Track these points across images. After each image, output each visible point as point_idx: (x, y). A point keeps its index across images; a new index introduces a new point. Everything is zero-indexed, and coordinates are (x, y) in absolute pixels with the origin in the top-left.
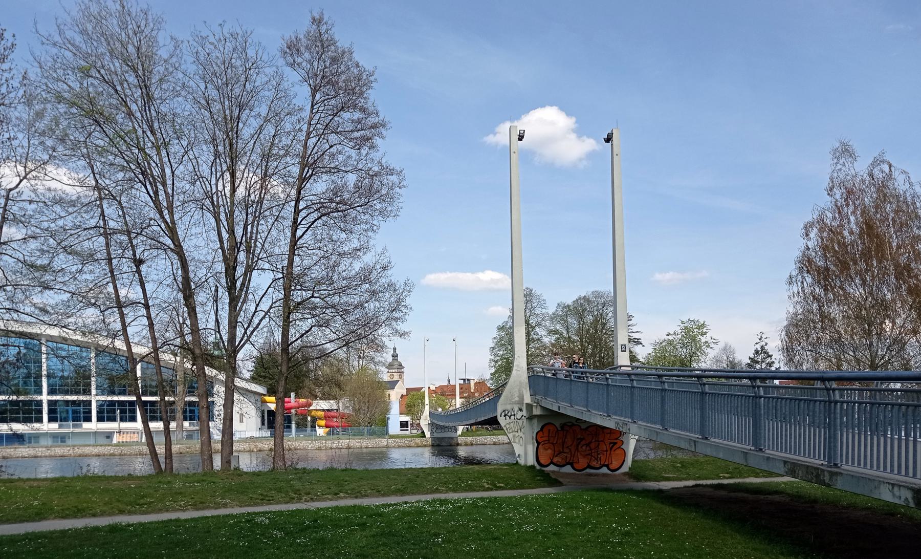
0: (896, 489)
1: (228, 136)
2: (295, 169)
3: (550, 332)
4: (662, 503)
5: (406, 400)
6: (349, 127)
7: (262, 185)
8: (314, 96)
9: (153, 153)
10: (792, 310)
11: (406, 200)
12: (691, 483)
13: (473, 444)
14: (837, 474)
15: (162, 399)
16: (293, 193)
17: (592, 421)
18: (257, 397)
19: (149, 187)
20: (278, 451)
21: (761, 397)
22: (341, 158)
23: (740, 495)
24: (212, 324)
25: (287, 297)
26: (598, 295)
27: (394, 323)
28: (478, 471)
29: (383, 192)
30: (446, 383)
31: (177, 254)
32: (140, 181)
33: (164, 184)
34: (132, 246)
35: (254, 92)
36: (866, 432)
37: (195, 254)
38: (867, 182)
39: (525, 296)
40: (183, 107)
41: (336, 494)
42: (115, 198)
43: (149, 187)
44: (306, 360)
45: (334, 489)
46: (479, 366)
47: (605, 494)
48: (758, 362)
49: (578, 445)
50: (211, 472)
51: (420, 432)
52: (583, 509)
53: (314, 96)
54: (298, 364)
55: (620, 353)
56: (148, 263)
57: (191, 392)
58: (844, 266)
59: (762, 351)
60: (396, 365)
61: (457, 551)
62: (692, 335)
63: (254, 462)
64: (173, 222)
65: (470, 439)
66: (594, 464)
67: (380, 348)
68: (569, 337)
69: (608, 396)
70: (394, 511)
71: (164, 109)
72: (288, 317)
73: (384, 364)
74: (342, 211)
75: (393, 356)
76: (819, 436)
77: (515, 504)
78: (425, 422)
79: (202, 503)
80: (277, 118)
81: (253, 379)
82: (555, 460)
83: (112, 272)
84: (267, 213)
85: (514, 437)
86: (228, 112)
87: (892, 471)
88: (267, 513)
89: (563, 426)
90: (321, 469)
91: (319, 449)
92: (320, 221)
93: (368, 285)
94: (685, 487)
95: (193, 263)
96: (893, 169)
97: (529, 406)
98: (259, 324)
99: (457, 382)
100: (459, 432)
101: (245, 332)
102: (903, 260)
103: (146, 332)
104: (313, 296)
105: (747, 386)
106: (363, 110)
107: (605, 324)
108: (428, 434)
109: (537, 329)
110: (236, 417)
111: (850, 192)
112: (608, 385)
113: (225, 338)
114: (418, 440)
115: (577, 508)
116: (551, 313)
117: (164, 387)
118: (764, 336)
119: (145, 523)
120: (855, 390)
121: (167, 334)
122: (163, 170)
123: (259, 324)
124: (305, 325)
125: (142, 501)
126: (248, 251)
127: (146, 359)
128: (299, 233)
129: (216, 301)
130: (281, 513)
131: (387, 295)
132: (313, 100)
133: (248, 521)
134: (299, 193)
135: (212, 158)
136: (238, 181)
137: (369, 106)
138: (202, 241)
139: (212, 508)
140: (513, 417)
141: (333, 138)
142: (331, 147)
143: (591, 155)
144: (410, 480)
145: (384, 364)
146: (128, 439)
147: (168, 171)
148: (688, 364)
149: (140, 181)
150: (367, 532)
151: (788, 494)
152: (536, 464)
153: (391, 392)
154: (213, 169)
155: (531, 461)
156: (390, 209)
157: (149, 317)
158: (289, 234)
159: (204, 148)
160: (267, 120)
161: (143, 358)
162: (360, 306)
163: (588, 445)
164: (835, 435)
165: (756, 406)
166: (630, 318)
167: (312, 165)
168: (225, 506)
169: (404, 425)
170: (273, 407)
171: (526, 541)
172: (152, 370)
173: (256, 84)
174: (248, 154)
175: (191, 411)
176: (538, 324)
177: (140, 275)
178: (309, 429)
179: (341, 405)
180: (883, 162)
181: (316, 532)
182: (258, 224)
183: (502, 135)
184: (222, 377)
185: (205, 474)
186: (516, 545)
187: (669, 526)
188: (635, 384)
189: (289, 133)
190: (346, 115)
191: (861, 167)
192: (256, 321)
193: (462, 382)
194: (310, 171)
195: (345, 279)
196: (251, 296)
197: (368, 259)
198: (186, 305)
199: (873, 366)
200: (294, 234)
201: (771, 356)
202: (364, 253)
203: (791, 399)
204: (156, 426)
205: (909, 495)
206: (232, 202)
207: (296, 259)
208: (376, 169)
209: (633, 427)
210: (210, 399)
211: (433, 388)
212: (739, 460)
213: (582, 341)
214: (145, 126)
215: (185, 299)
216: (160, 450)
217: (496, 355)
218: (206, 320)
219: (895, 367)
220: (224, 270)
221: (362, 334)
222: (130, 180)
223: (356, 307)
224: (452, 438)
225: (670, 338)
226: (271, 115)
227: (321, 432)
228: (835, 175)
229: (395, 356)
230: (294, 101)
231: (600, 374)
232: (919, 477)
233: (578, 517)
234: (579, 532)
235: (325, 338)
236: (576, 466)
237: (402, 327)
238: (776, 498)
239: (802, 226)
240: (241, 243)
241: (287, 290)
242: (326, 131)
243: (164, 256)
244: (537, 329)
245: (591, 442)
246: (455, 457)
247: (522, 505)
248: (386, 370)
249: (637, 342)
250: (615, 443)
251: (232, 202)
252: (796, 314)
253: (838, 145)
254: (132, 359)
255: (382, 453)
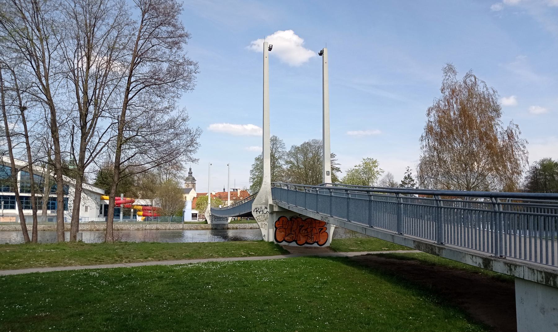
0: (474, 258)
1: (87, 35)
2: (129, 57)
3: (287, 162)
4: (347, 265)
5: (197, 201)
6: (165, 35)
7: (107, 65)
8: (143, 15)
9: (37, 43)
10: (423, 156)
11: (199, 80)
12: (365, 253)
13: (245, 231)
14: (442, 248)
15: (33, 195)
16: (128, 72)
17: (308, 215)
18: (96, 196)
19: (33, 63)
20: (108, 231)
21: (401, 204)
22: (159, 53)
23: (392, 260)
24: (68, 149)
25: (120, 134)
26: (316, 142)
27: (189, 153)
28: (239, 245)
29: (185, 75)
30: (222, 191)
31: (49, 105)
32: (28, 59)
33: (44, 62)
34: (20, 98)
35: (106, 11)
36: (461, 225)
37: (60, 105)
38: (463, 86)
39: (272, 140)
40: (59, 16)
41: (146, 258)
42: (10, 69)
43: (33, 63)
44: (132, 173)
45: (145, 255)
46: (242, 181)
47: (314, 259)
48: (406, 184)
49: (300, 230)
50: (64, 243)
51: (204, 220)
52: (300, 268)
53: (143, 15)
54: (126, 176)
55: (326, 176)
56: (29, 109)
57: (53, 192)
58: (450, 132)
59: (409, 177)
60: (191, 179)
61: (220, 294)
62: (369, 168)
63: (92, 238)
64: (48, 85)
65: (236, 225)
66: (309, 241)
67: (179, 168)
68: (298, 166)
69: (331, 202)
70: (182, 269)
71: (46, 17)
72: (120, 147)
73: (183, 178)
74: (158, 85)
75: (189, 173)
76: (433, 226)
77: (259, 265)
78: (207, 215)
79: (55, 262)
80: (120, 27)
81: (96, 185)
82: (286, 238)
83: (4, 114)
84: (110, 83)
85: (262, 224)
86: (88, 21)
87: (472, 248)
88: (98, 269)
89: (291, 219)
90: (137, 242)
91: (138, 230)
92: (144, 90)
93: (173, 130)
94: (362, 255)
95: (58, 111)
96: (477, 80)
97: (271, 206)
98: (100, 151)
99: (229, 190)
100: (229, 221)
101: (91, 155)
102: (483, 130)
103: (25, 152)
104: (137, 135)
105: (397, 198)
106: (174, 26)
107: (319, 159)
108: (209, 222)
109: (279, 160)
110: (82, 209)
111: (453, 91)
112: (317, 194)
113: (77, 158)
114: (203, 226)
115: (296, 267)
116: (288, 151)
117: (33, 186)
118: (410, 169)
119: (14, 275)
120: (459, 201)
121: (39, 155)
122: (44, 53)
123: (100, 151)
124: (130, 153)
125: (14, 261)
126: (96, 105)
127: (24, 169)
128: (130, 96)
129: (73, 135)
130: (107, 270)
131: (185, 136)
132: (143, 18)
133: (85, 275)
134: (131, 72)
135: (76, 48)
136: (91, 63)
137: (178, 24)
138: (65, 98)
139: (62, 266)
140: (261, 212)
141: (154, 41)
142: (153, 46)
143: (311, 59)
144: (195, 250)
145: (183, 178)
146: (9, 221)
147: (47, 54)
148: (367, 183)
149: (28, 59)
150: (164, 282)
151: (419, 260)
152: (275, 241)
153: (187, 195)
154: (76, 54)
155: (272, 239)
156: (189, 85)
157: (27, 143)
158: (123, 96)
159: (71, 41)
160: (113, 27)
161: (22, 169)
162: (168, 142)
163: (306, 230)
164: (441, 226)
165: (399, 209)
166: (332, 156)
167: (140, 56)
168: (71, 265)
169: (194, 216)
170: (107, 202)
171: (264, 287)
172: (28, 176)
173: (107, 6)
174: (99, 47)
175: (52, 204)
176: (280, 158)
177: (23, 117)
178: (132, 217)
179: (154, 203)
180: (471, 76)
181: (129, 282)
182: (103, 89)
183: (259, 45)
184: (74, 182)
185: (59, 244)
186: (257, 290)
187: (349, 278)
188: (333, 194)
189: (126, 36)
190: (164, 28)
191: (459, 78)
192: (98, 148)
193: (232, 190)
194: (139, 60)
195: (158, 125)
196: (96, 133)
197: (174, 114)
198: (53, 137)
199: (468, 188)
200: (127, 96)
201: (413, 180)
202: (172, 111)
203: (425, 206)
204: (28, 212)
205: (480, 261)
206: (87, 75)
207: (128, 111)
208: (181, 61)
209: (331, 220)
210: (65, 196)
211: (214, 193)
212: (389, 239)
213: (305, 168)
214: (34, 27)
215: (52, 133)
216: (30, 227)
217: (254, 175)
218: (65, 146)
219: (481, 190)
220: (79, 115)
221: (169, 158)
222: (20, 58)
223: (165, 143)
224: (224, 224)
225: (357, 168)
226: (115, 24)
227: (139, 219)
228: (446, 82)
229: (190, 173)
230: (130, 17)
231: (314, 188)
232: (556, 264)
233: (297, 273)
234: (296, 282)
235: (145, 161)
236: (298, 242)
237: (194, 156)
238: (412, 262)
239: (427, 109)
240: (91, 100)
241: (121, 131)
242: (150, 37)
243: (40, 105)
244: (279, 160)
245: (308, 228)
246: (225, 237)
247: (263, 266)
248: (184, 182)
249: (338, 170)
250: (322, 229)
251: (87, 75)
252: (425, 157)
253: (446, 66)
254: (15, 170)
255: (180, 233)
